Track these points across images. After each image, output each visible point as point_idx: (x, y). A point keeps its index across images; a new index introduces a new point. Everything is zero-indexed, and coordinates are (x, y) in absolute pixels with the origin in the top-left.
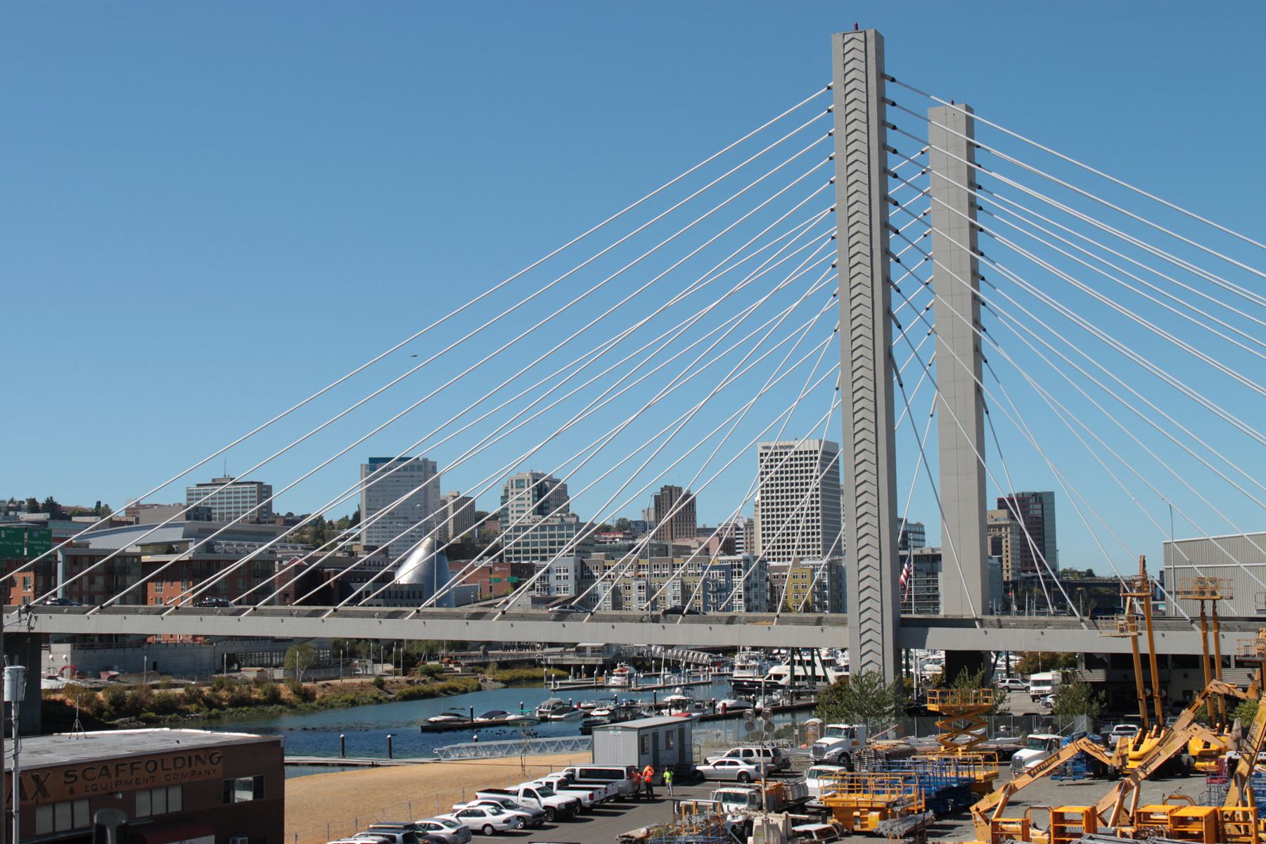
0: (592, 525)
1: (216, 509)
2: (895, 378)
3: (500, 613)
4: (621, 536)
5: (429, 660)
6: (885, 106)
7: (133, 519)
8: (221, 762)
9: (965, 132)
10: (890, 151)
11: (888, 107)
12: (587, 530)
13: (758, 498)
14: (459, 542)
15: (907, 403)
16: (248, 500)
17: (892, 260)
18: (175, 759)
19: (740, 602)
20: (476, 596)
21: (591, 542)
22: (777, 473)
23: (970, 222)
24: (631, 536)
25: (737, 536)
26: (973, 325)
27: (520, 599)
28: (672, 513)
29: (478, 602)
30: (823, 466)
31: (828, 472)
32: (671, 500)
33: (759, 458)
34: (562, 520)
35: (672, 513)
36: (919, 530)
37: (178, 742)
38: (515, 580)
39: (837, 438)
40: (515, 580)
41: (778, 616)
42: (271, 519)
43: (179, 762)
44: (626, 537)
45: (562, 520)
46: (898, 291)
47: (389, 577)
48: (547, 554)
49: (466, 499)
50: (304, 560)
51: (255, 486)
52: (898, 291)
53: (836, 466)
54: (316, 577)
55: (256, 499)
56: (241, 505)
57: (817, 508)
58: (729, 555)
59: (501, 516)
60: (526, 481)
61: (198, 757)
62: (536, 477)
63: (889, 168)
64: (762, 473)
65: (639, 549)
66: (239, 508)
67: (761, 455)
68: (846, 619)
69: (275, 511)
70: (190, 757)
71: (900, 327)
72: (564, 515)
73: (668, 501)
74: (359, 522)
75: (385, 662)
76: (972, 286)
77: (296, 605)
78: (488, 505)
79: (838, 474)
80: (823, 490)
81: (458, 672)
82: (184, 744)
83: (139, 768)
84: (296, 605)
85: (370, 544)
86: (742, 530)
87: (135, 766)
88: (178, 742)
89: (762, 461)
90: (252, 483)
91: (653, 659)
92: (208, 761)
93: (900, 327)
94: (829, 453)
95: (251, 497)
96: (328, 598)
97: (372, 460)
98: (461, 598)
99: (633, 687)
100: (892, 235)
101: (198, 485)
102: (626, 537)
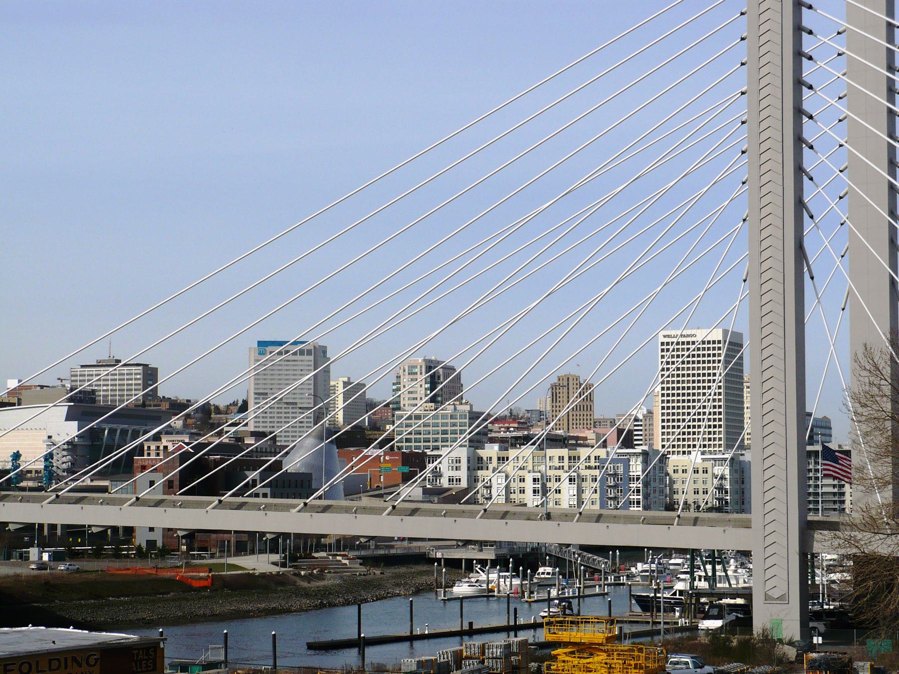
0: (489, 415)
1: (100, 390)
2: (806, 269)
3: (390, 508)
4: (516, 425)
5: (317, 551)
6: (801, 36)
7: (15, 400)
8: (98, 663)
9: (885, 12)
10: (805, 7)
11: (804, 10)
12: (485, 420)
13: (659, 389)
14: (350, 430)
15: (817, 295)
16: (133, 387)
17: (804, 146)
18: (50, 661)
19: (638, 497)
20: (365, 485)
21: (486, 430)
22: (683, 362)
23: (888, 107)
24: (525, 426)
25: (636, 428)
26: (889, 216)
27: (411, 491)
28: (568, 407)
29: (368, 491)
30: (727, 362)
31: (731, 369)
32: (568, 397)
33: (660, 354)
34: (455, 409)
35: (568, 407)
36: (825, 425)
37: (54, 642)
38: (406, 469)
39: (743, 327)
40: (406, 469)
41: (679, 516)
42: (156, 402)
43: (55, 664)
44: (521, 426)
45: (455, 409)
46: (811, 179)
47: (278, 465)
48: (440, 444)
49: (361, 386)
50: (191, 448)
51: (141, 368)
52: (811, 179)
53: (740, 363)
54: (201, 466)
55: (141, 387)
56: (125, 387)
57: (720, 420)
58: (627, 448)
59: (395, 405)
60: (419, 367)
61: (74, 659)
62: (430, 365)
63: (803, 50)
64: (663, 370)
65: (539, 439)
66: (124, 390)
67: (662, 344)
68: (749, 521)
69: (160, 394)
70: (66, 659)
71: (812, 217)
72: (458, 403)
73: (566, 397)
74: (247, 410)
75: (271, 552)
76: (889, 174)
77: (180, 494)
78: (379, 393)
79: (742, 371)
80: (726, 388)
81: (346, 564)
82: (60, 645)
83: (13, 670)
84: (180, 494)
85: (257, 430)
86: (641, 421)
87: (9, 667)
88: (54, 642)
89: (663, 357)
90: (138, 365)
91: (547, 554)
92: (84, 663)
93: (812, 217)
94: (735, 346)
95: (136, 384)
96: (211, 488)
97: (261, 344)
98: (353, 489)
99: (526, 599)
100: (805, 119)
101: (82, 366)
102: (521, 426)
